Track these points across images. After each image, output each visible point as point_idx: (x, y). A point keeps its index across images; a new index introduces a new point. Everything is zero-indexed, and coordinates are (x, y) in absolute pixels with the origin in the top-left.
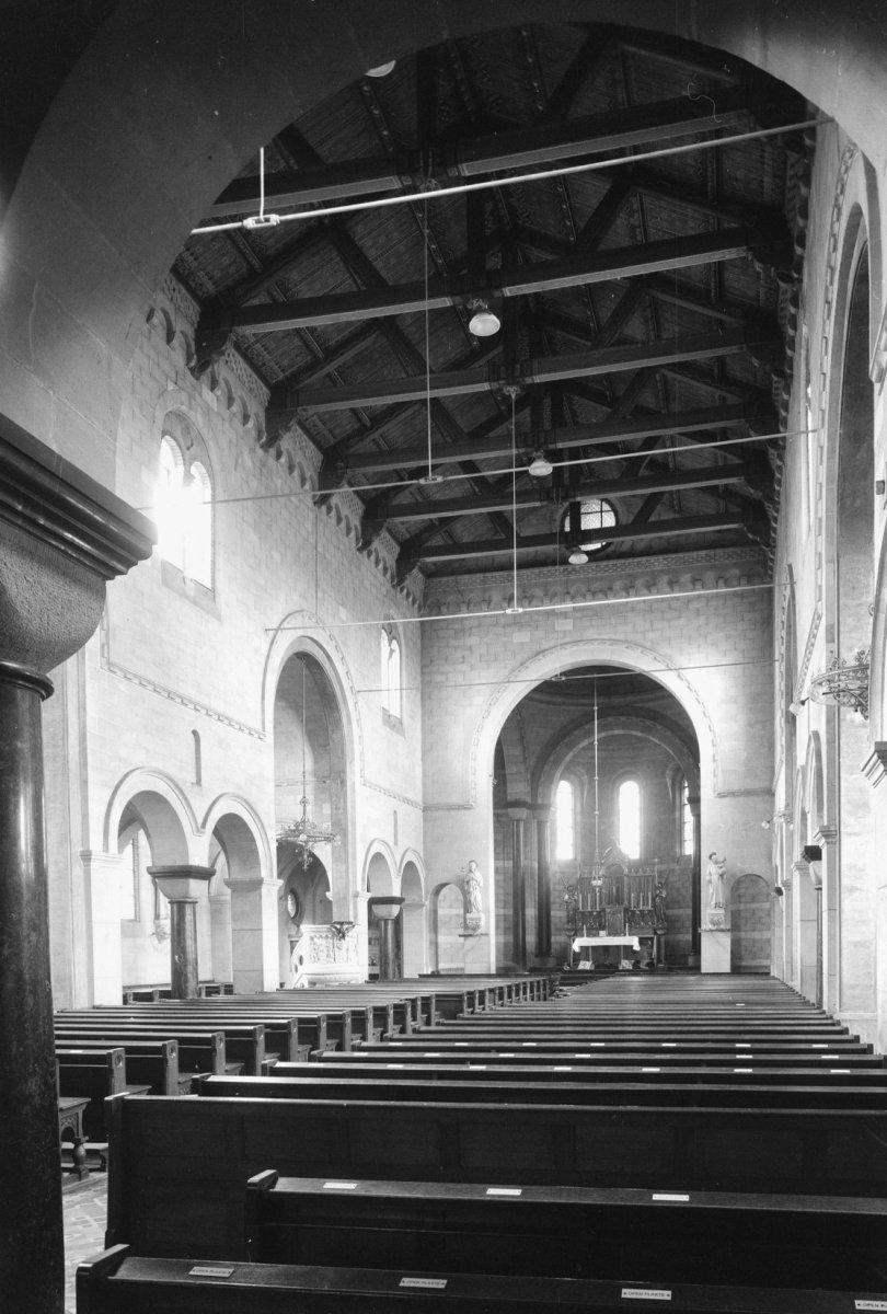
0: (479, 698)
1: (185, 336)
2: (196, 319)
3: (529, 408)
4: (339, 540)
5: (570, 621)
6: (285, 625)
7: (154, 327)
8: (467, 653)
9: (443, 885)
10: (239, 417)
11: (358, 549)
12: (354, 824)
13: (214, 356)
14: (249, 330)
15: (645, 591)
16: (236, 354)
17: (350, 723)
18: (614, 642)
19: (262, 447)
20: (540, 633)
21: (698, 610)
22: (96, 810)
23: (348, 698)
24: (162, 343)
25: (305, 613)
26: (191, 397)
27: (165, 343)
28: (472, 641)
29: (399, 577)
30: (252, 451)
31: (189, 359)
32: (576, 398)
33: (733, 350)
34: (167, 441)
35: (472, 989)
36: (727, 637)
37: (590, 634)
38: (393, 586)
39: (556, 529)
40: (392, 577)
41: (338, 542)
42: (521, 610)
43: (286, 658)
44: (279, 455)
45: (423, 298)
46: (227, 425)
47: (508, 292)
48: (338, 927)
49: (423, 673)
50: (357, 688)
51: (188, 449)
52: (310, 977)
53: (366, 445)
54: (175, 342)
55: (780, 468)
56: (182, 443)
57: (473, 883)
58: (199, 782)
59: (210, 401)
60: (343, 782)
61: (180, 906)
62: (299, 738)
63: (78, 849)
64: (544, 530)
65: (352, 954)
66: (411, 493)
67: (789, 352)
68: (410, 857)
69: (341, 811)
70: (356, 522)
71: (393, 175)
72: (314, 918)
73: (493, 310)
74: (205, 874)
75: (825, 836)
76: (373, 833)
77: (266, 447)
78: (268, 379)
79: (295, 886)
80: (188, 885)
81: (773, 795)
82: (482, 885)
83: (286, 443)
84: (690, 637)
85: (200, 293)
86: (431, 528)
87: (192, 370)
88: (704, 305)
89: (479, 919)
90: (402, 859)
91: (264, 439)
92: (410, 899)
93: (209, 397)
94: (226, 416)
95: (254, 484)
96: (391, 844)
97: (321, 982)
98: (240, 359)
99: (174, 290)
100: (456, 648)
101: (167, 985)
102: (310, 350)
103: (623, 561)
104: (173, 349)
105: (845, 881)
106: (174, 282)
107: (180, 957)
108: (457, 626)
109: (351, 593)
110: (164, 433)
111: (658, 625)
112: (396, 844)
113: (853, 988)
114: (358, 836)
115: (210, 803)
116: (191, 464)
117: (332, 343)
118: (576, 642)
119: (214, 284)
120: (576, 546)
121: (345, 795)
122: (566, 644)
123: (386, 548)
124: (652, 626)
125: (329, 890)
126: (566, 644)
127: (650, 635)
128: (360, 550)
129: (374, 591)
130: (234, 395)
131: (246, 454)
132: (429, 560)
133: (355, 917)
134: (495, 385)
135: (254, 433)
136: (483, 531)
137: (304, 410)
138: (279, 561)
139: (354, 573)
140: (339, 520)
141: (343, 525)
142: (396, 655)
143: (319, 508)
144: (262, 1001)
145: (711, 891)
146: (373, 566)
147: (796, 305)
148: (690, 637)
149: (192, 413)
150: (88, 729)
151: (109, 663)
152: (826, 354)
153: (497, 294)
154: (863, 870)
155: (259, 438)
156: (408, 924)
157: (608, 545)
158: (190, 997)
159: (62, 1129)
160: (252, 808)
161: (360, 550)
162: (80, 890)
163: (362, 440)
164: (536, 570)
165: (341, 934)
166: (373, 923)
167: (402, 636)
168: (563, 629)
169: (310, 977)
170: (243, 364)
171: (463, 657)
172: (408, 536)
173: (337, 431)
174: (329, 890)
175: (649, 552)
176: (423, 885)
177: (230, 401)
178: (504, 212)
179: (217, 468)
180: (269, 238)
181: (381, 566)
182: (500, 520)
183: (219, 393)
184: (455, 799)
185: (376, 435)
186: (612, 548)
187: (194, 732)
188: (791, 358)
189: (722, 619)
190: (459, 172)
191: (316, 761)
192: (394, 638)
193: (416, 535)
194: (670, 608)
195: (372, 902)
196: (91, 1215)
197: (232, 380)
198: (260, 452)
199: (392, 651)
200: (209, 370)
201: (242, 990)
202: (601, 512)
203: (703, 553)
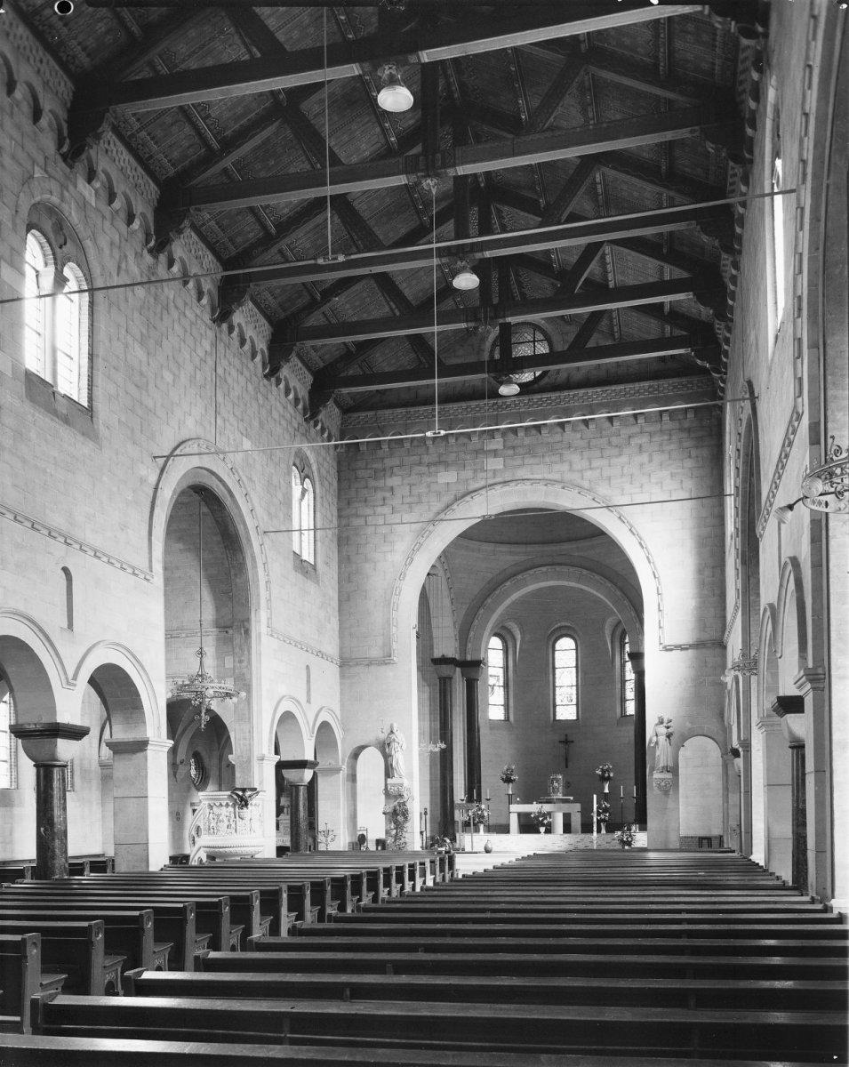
0: (402, 546)
1: (56, 117)
2: (68, 97)
3: (453, 220)
4: (242, 363)
6: (177, 452)
7: (41, 130)
8: (388, 495)
9: (363, 748)
10: (123, 215)
11: (266, 376)
13: (321, 408)
14: (131, 110)
16: (118, 143)
17: (255, 567)
18: (548, 482)
19: (150, 251)
20: (468, 473)
21: (641, 446)
23: (253, 539)
24: (26, 122)
25: (201, 442)
26: (63, 187)
27: (31, 122)
28: (394, 481)
29: (312, 409)
30: (138, 255)
31: (60, 145)
32: (506, 208)
33: (683, 133)
34: (33, 235)
35: (388, 866)
37: (521, 473)
38: (306, 420)
39: (486, 357)
40: (305, 409)
41: (243, 374)
42: (443, 433)
43: (179, 491)
44: (278, 382)
45: (321, 67)
46: (107, 224)
47: (426, 56)
48: (240, 793)
49: (340, 517)
50: (263, 528)
51: (61, 247)
53: (315, 320)
54: (44, 122)
55: (734, 279)
56: (54, 243)
57: (394, 745)
58: (70, 626)
59: (86, 194)
60: (247, 632)
61: (47, 772)
64: (472, 359)
65: (256, 825)
66: (325, 315)
67: (749, 131)
68: (324, 717)
69: (245, 664)
70: (262, 345)
71: (354, 62)
72: (220, 785)
73: (475, 270)
74: (77, 733)
75: (811, 681)
77: (154, 252)
78: (140, 153)
79: (199, 749)
81: (725, 648)
83: (178, 249)
85: (72, 67)
86: (348, 355)
87: (64, 157)
88: (650, 83)
90: (315, 720)
91: (152, 243)
92: (323, 763)
93: (86, 190)
94: (108, 215)
96: (303, 700)
97: (222, 855)
98: (122, 148)
99: (41, 61)
100: (376, 489)
101: (30, 861)
102: (127, 29)
103: (557, 394)
104: (41, 130)
106: (41, 53)
107: (46, 830)
108: (374, 466)
109: (256, 424)
110: (29, 228)
111: (596, 463)
112: (309, 701)
114: (264, 693)
115: (84, 651)
116: (63, 265)
117: (229, 133)
119: (88, 55)
120: (506, 375)
123: (296, 376)
127: (588, 474)
128: (267, 377)
129: (283, 422)
130: (116, 190)
131: (131, 258)
132: (345, 391)
133: (261, 783)
134: (413, 178)
135: (141, 236)
136: (406, 360)
137: (257, 285)
138: (171, 382)
139: (261, 402)
140: (243, 342)
141: (247, 347)
142: (309, 496)
143: (219, 326)
144: (144, 881)
146: (283, 395)
147: (747, 184)
149: (65, 207)
153: (412, 59)
155: (147, 242)
156: (323, 787)
157: (544, 374)
158: (57, 877)
160: (135, 657)
161: (267, 377)
163: (267, 250)
164: (464, 405)
165: (244, 803)
166: (282, 787)
167: (316, 474)
168: (493, 468)
169: (208, 849)
170: (126, 156)
172: (322, 365)
173: (239, 239)
174: (231, 753)
175: (587, 383)
177: (111, 197)
178: (455, 87)
180: (284, 208)
181: (291, 396)
182: (419, 343)
183: (97, 185)
184: (375, 653)
185: (326, 308)
186: (546, 380)
187: (65, 570)
188: (751, 139)
189: (667, 456)
190: (419, 58)
191: (218, 609)
192: (307, 476)
193: (331, 364)
194: (610, 443)
195: (280, 766)
197: (114, 175)
198: (148, 259)
199: (304, 491)
200: (83, 156)
201: (123, 867)
202: (534, 341)
203: (646, 384)
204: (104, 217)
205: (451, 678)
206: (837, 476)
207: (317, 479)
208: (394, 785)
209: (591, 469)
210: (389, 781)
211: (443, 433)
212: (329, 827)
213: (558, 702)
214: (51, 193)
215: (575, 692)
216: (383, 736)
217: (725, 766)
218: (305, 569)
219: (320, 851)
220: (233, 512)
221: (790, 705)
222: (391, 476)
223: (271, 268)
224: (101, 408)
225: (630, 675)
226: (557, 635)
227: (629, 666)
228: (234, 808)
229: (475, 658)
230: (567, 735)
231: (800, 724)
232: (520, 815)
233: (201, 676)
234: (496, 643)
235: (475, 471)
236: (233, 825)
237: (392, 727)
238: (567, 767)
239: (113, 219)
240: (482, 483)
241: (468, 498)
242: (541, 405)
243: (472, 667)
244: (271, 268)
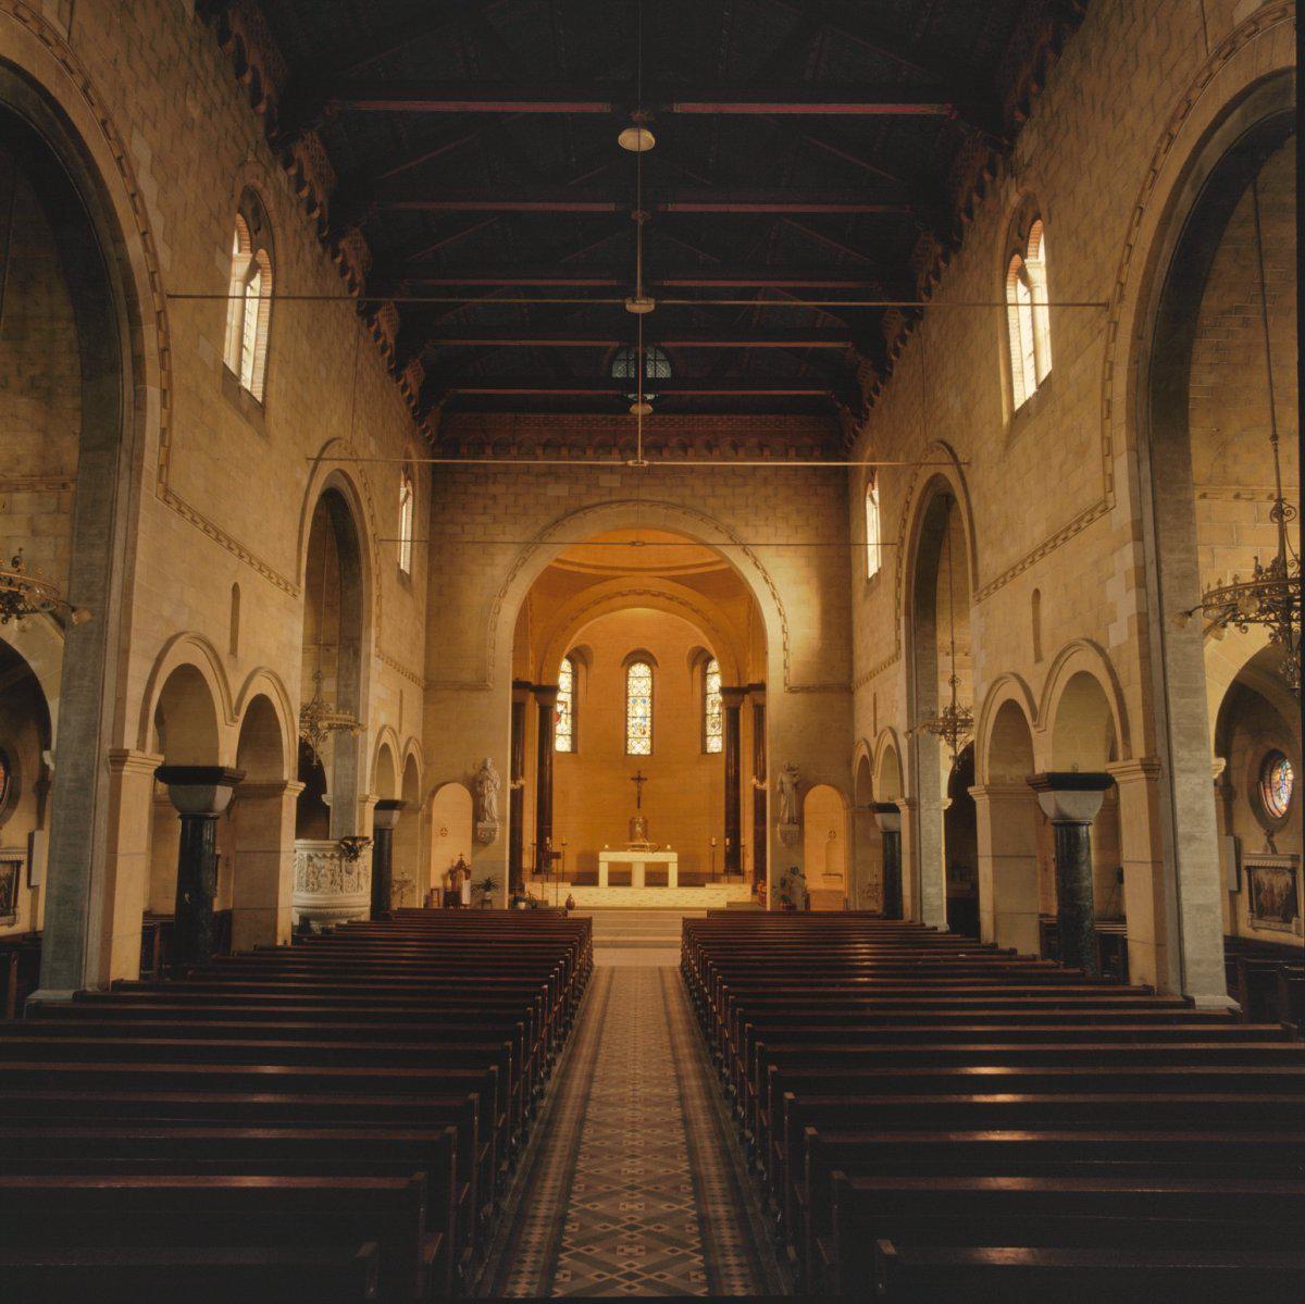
0: (503, 559)
5: (618, 477)
8: (490, 503)
12: (367, 705)
15: (705, 453)
22: (135, 691)
26: (267, 173)
29: (419, 413)
36: (799, 512)
42: (646, 463)
46: (294, 211)
49: (432, 522)
51: (256, 233)
52: (300, 910)
59: (282, 179)
60: (357, 653)
63: (107, 747)
75: (1146, 771)
76: (383, 719)
80: (214, 794)
82: (498, 784)
84: (757, 507)
89: (494, 830)
94: (295, 202)
95: (311, 283)
100: (476, 495)
105: (1181, 829)
113: (1198, 963)
118: (622, 502)
121: (358, 667)
122: (611, 502)
124: (713, 492)
125: (325, 792)
126: (611, 502)
127: (711, 501)
128: (390, 372)
145: (783, 803)
148: (757, 507)
150: (136, 579)
151: (167, 491)
154: (1202, 815)
162: (103, 806)
169: (300, 910)
171: (485, 508)
176: (420, 784)
179: (281, 259)
184: (467, 676)
198: (319, 248)
204: (292, 205)
205: (524, 704)
206: (1265, 595)
207: (417, 481)
208: (483, 830)
209: (714, 496)
210: (480, 825)
211: (646, 463)
212: (407, 876)
213: (630, 733)
214: (258, 178)
215: (649, 724)
216: (471, 772)
218: (404, 579)
220: (357, 517)
222: (493, 483)
224: (272, 403)
226: (644, 658)
228: (340, 860)
230: (639, 772)
232: (611, 864)
233: (316, 703)
234: (566, 665)
235: (589, 486)
236: (339, 881)
237: (485, 762)
238: (639, 807)
239: (298, 206)
240: (596, 500)
241: (580, 514)
242: (663, 426)
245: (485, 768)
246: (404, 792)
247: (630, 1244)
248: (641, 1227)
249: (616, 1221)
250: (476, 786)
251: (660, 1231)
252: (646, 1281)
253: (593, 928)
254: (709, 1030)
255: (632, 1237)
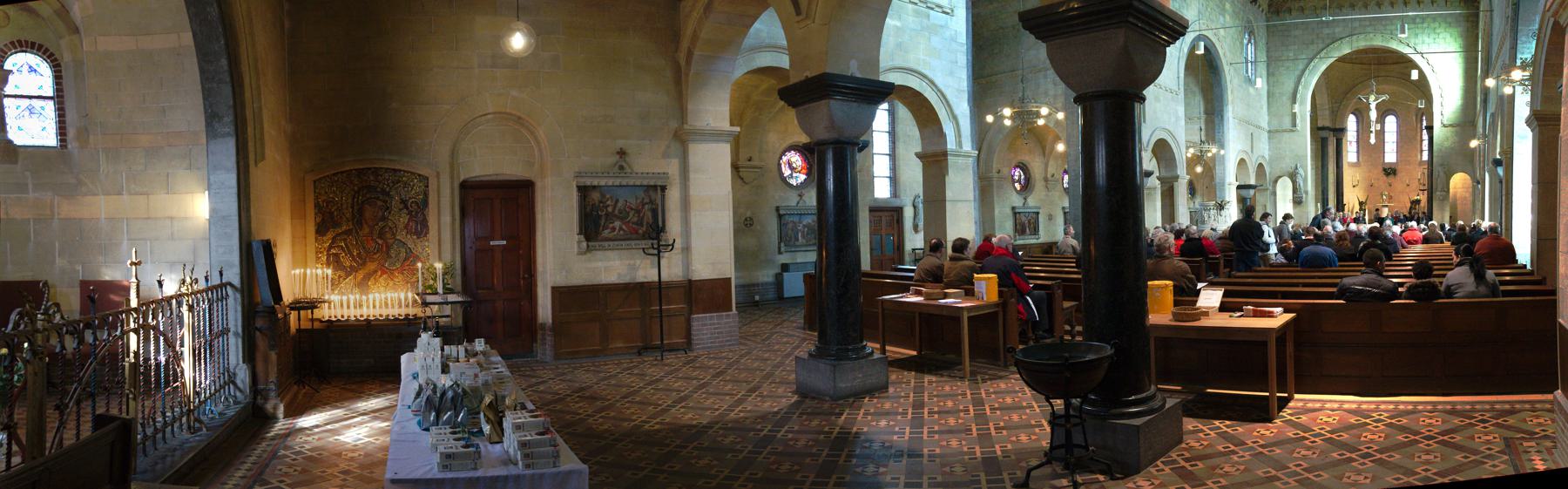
50: (1230, 61)
60: (1222, 117)
62: (1197, 94)
112: (1252, 152)
152: (973, 476)
159: (882, 356)
195: (1239, 187)
196: (1037, 403)
205: (1327, 138)
217: (1474, 187)
219: (787, 298)
221: (1497, 163)
223: (1476, 300)
225: (1425, 136)
227: (1425, 132)
229: (1341, 127)
231: (1500, 171)
243: (1340, 132)
244: (1476, 300)
245: (1297, 168)
246: (1257, 179)
247: (1428, 453)
248: (1436, 438)
249: (1416, 433)
250: (1293, 176)
251: (1452, 441)
252: (1478, 454)
253: (188, 38)
254: (97, 343)
255: (1428, 445)
